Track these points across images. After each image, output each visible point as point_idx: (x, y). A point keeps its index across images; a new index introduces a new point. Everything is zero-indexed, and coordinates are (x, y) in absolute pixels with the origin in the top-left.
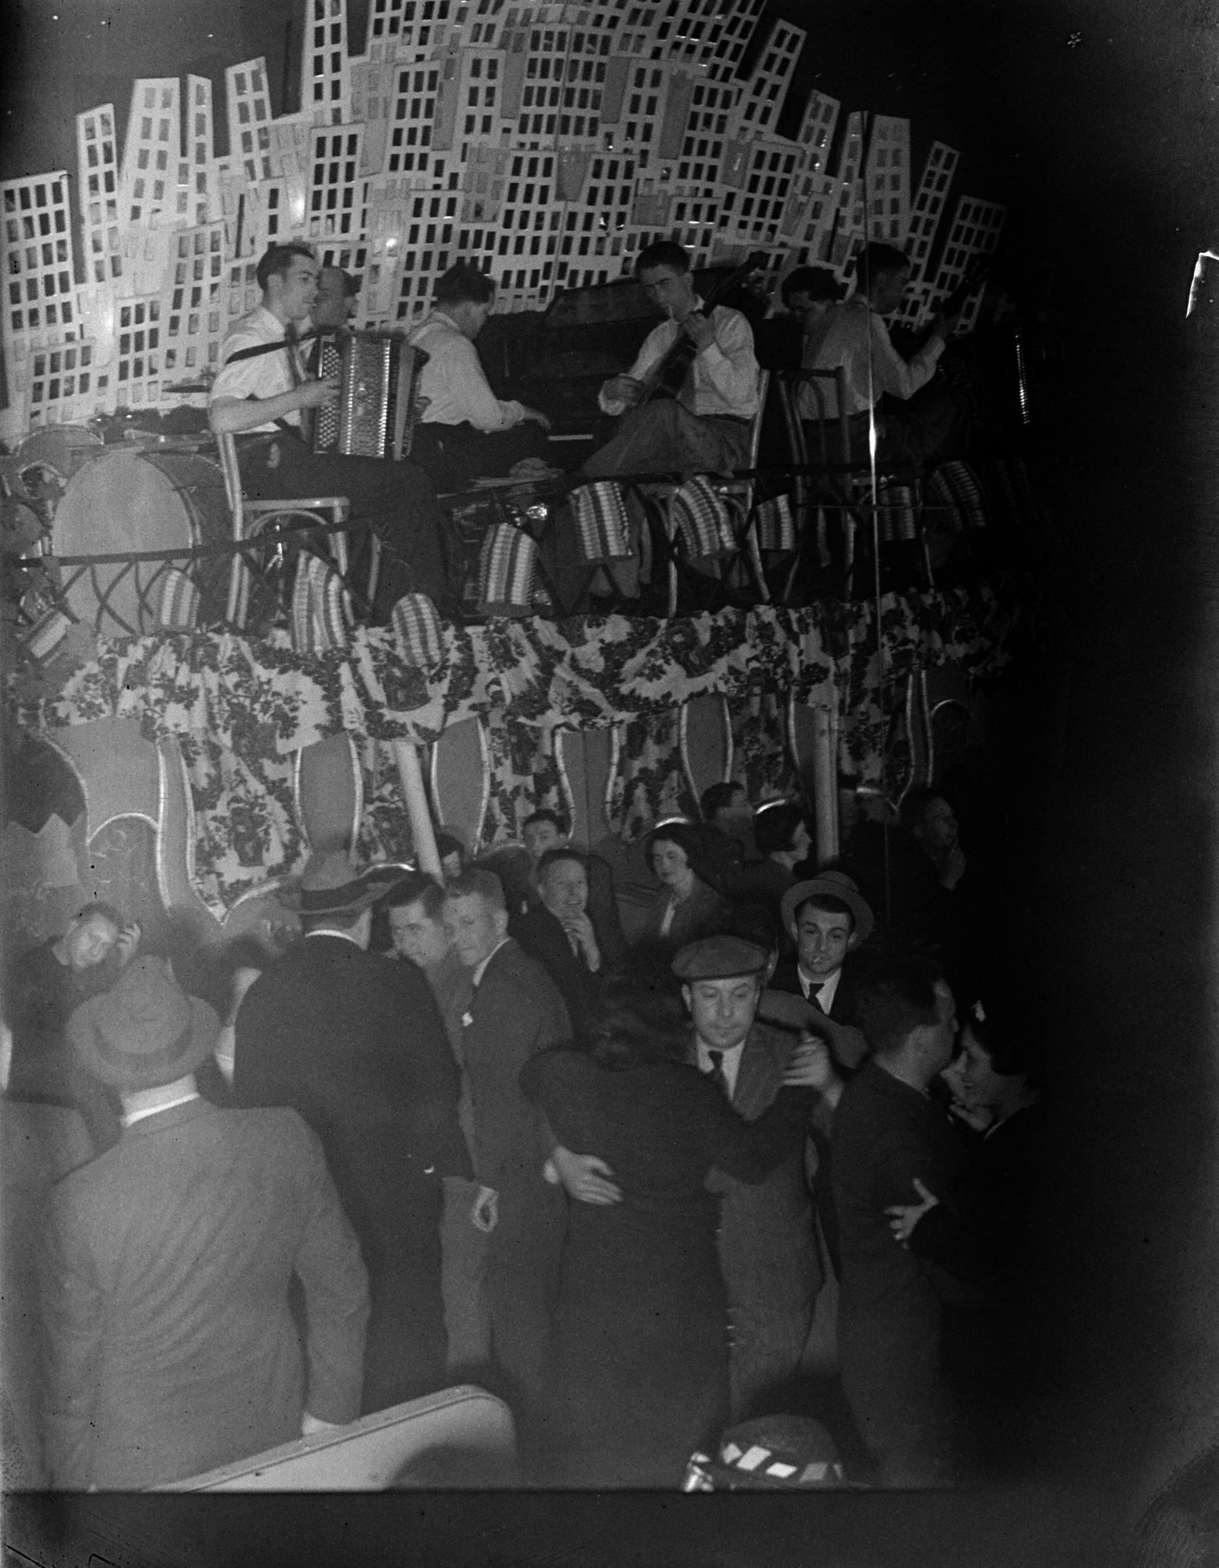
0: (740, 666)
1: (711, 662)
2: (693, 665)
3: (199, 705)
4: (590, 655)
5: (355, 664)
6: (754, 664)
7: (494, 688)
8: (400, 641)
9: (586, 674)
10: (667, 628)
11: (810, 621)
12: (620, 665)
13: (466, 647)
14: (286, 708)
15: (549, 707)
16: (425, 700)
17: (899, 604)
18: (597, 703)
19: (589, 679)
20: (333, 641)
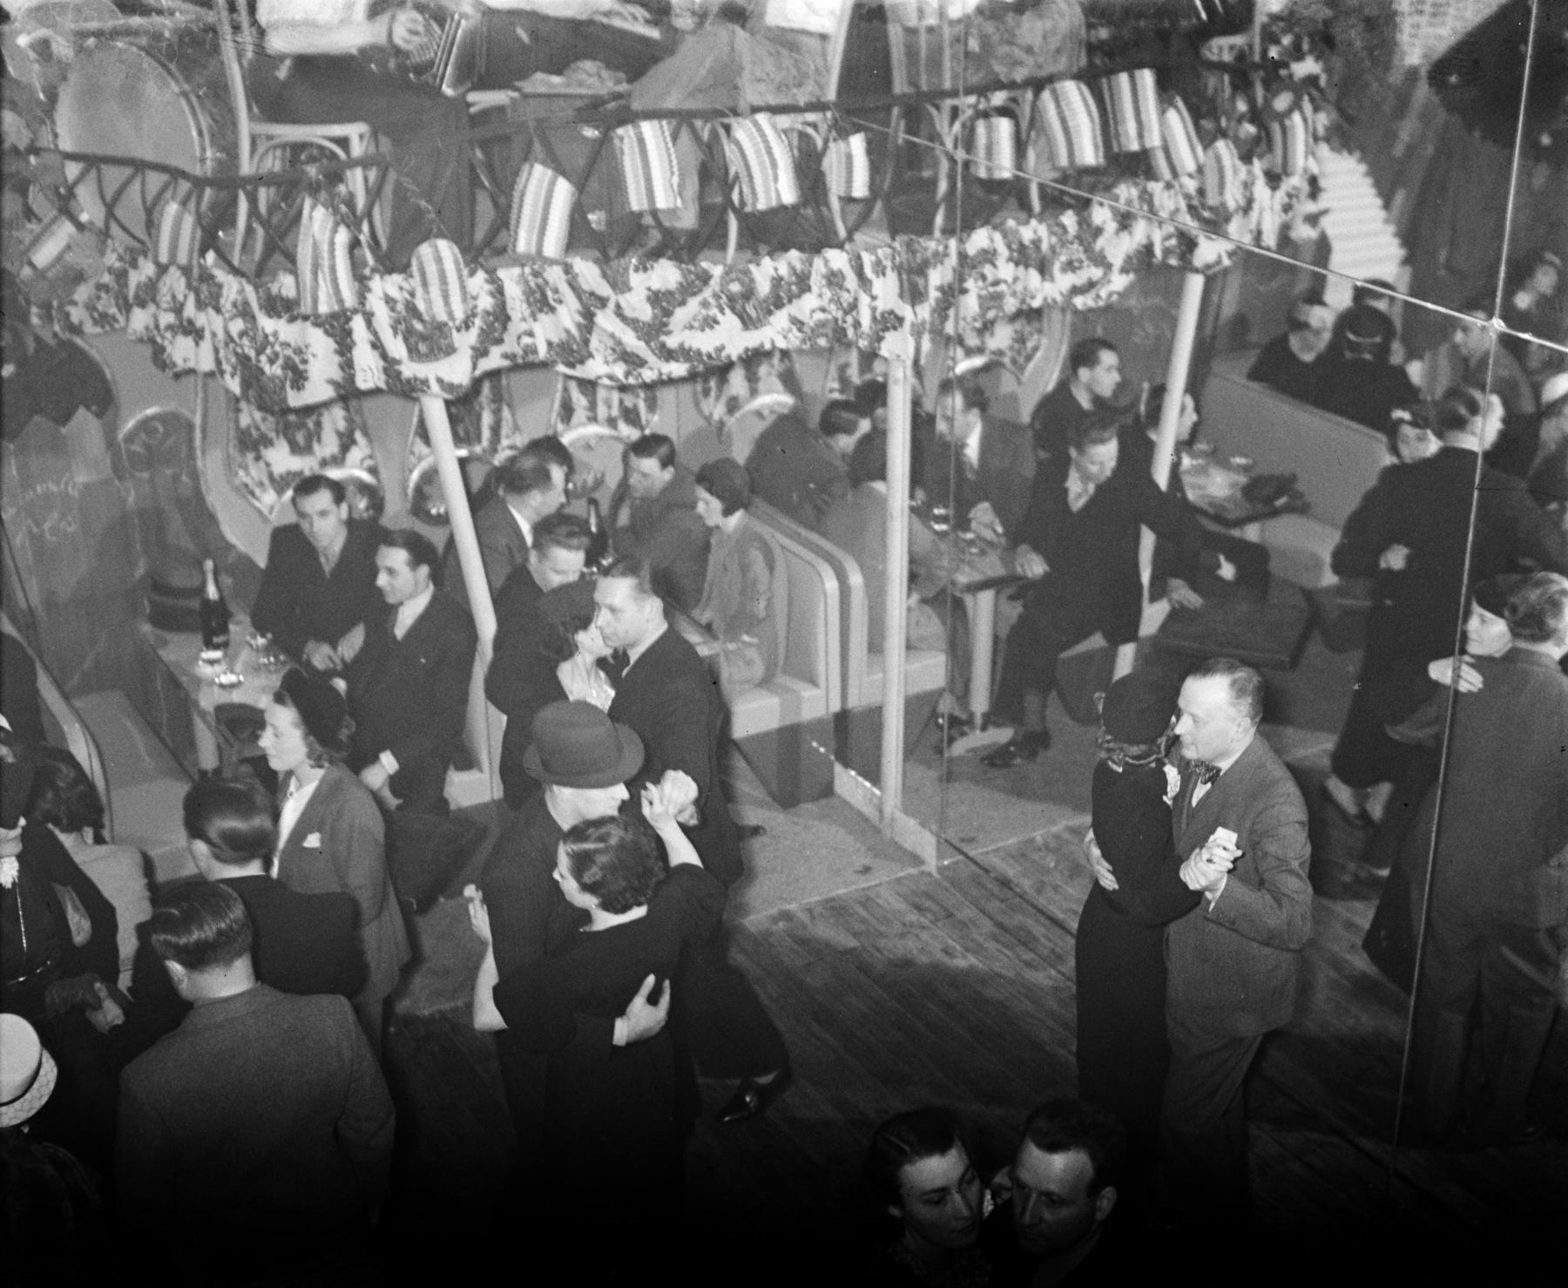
0: (804, 317)
1: (770, 313)
2: (750, 318)
3: (206, 345)
4: (637, 304)
5: (369, 318)
6: (820, 316)
7: (526, 340)
8: (419, 292)
9: (632, 323)
10: (722, 278)
11: (888, 264)
12: (668, 313)
13: (499, 292)
14: (297, 359)
15: (591, 356)
16: (450, 350)
17: (992, 240)
18: (641, 354)
19: (635, 329)
20: (341, 301)
